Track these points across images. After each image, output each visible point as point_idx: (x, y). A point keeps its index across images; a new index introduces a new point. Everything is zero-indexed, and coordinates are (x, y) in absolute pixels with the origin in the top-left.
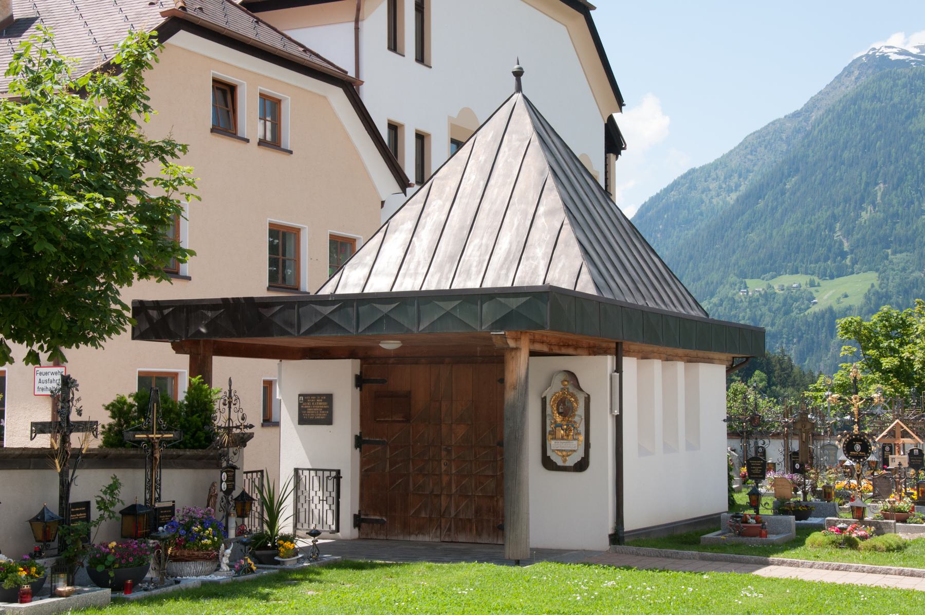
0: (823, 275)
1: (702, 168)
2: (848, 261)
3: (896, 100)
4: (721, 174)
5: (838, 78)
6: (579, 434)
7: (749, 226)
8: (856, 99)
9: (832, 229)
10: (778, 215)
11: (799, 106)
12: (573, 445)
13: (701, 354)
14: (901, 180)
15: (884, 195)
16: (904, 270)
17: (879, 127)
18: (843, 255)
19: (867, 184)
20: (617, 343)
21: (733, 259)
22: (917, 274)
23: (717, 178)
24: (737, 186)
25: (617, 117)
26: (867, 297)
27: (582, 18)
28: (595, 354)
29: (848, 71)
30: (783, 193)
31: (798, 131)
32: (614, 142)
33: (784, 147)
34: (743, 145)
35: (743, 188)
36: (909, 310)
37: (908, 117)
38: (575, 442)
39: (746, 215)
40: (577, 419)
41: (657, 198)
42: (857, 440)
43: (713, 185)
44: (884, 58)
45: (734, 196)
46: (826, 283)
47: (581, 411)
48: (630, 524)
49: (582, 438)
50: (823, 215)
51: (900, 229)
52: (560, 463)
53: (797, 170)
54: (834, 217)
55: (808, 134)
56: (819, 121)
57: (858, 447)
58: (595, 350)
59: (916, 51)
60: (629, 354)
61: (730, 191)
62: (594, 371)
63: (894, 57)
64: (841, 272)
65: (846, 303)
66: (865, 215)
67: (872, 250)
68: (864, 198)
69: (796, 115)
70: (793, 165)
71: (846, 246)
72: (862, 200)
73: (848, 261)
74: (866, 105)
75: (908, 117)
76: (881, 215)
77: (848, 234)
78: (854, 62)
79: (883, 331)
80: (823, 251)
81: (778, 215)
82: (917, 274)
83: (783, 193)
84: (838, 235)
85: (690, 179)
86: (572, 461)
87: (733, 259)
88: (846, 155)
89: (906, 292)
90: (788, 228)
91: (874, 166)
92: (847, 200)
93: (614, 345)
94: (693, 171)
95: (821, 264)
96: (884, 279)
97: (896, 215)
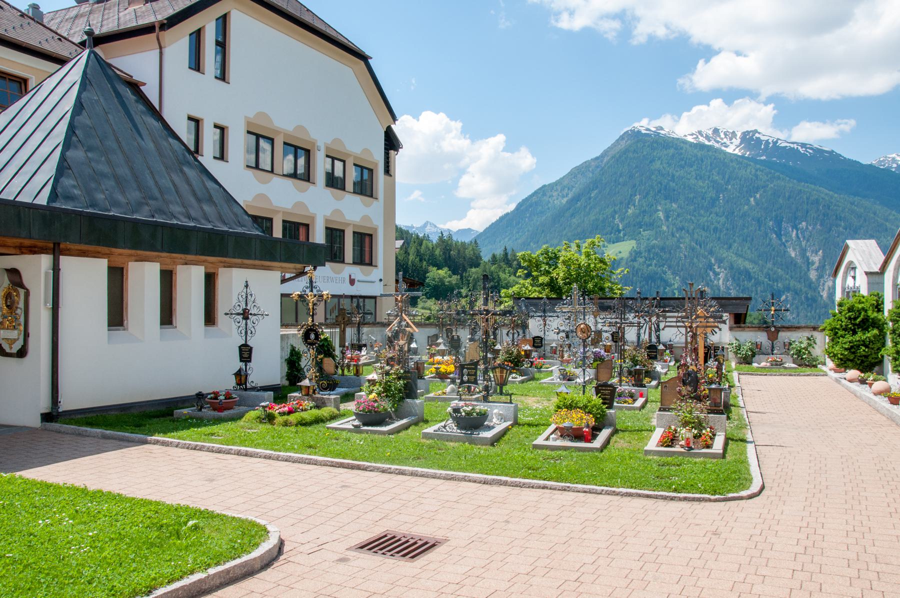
0: (609, 242)
1: (549, 185)
2: (621, 235)
3: (645, 153)
4: (559, 188)
5: (617, 141)
6: (19, 325)
7: (572, 215)
8: (626, 151)
9: (614, 218)
10: (587, 210)
11: (598, 154)
12: (14, 334)
13: (92, 248)
14: (647, 194)
15: (639, 201)
16: (648, 239)
17: (637, 167)
18: (619, 231)
19: (631, 195)
20: (54, 244)
21: (564, 233)
22: (654, 242)
23: (557, 190)
24: (567, 195)
25: (393, 126)
26: (630, 253)
27: (362, 63)
28: (34, 253)
29: (622, 138)
30: (590, 198)
31: (597, 167)
32: (391, 143)
33: (591, 175)
34: (570, 173)
35: (570, 196)
36: (558, 248)
37: (651, 162)
38: (16, 332)
39: (571, 211)
40: (19, 311)
41: (525, 201)
42: (311, 330)
43: (555, 194)
44: (639, 132)
45: (565, 199)
46: (611, 246)
47: (21, 305)
48: (67, 403)
49: (22, 328)
50: (609, 211)
51: (647, 219)
52: (8, 350)
53: (597, 187)
54: (615, 212)
55: (603, 168)
56: (608, 162)
57: (312, 336)
58: (34, 250)
59: (654, 129)
60: (69, 253)
61: (563, 197)
62: (36, 268)
63: (644, 132)
64: (618, 240)
65: (620, 256)
66: (630, 211)
67: (633, 229)
68: (630, 202)
69: (597, 158)
70: (595, 184)
71: (621, 227)
72: (629, 204)
73: (621, 235)
74: (631, 155)
75: (651, 162)
76: (638, 211)
77: (622, 220)
78: (625, 133)
79: (545, 261)
80: (609, 229)
81: (587, 210)
82: (654, 242)
83: (590, 198)
84: (617, 221)
85: (543, 191)
86: (15, 350)
87: (564, 233)
88: (621, 180)
89: (649, 251)
90: (592, 217)
91: (634, 186)
92: (621, 203)
93: (52, 245)
94: (544, 186)
95: (608, 236)
96: (639, 244)
97: (645, 211)
